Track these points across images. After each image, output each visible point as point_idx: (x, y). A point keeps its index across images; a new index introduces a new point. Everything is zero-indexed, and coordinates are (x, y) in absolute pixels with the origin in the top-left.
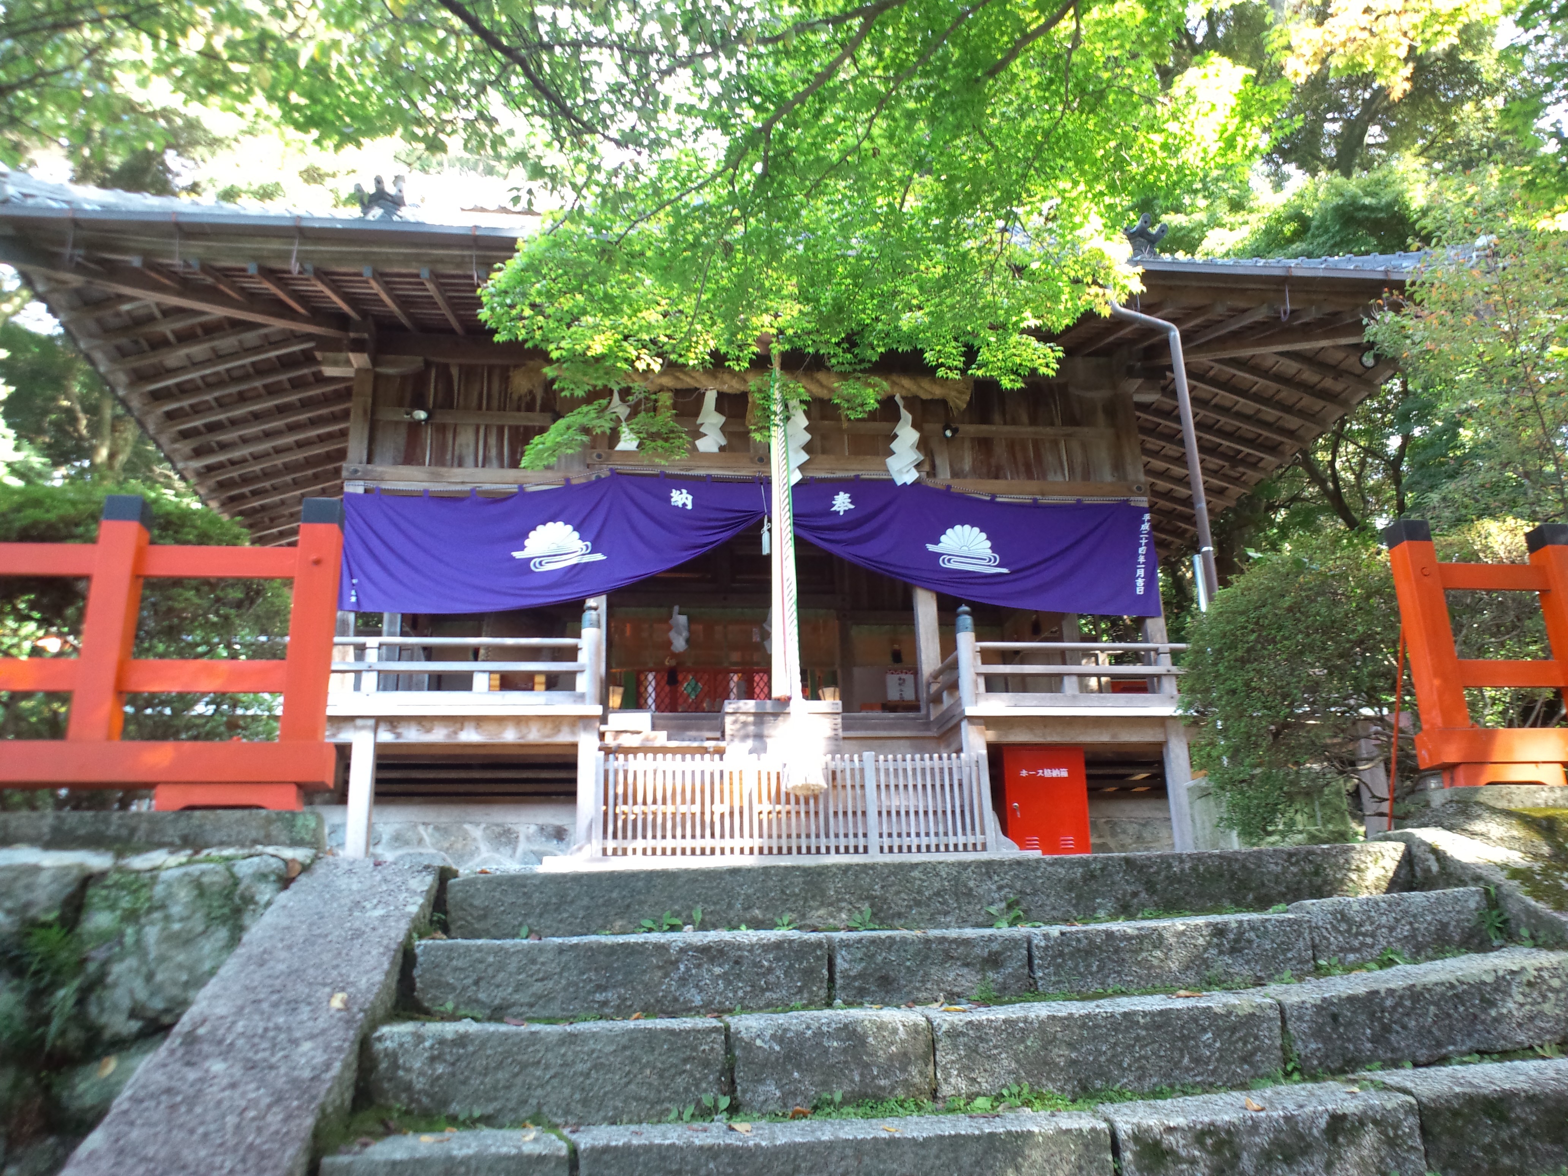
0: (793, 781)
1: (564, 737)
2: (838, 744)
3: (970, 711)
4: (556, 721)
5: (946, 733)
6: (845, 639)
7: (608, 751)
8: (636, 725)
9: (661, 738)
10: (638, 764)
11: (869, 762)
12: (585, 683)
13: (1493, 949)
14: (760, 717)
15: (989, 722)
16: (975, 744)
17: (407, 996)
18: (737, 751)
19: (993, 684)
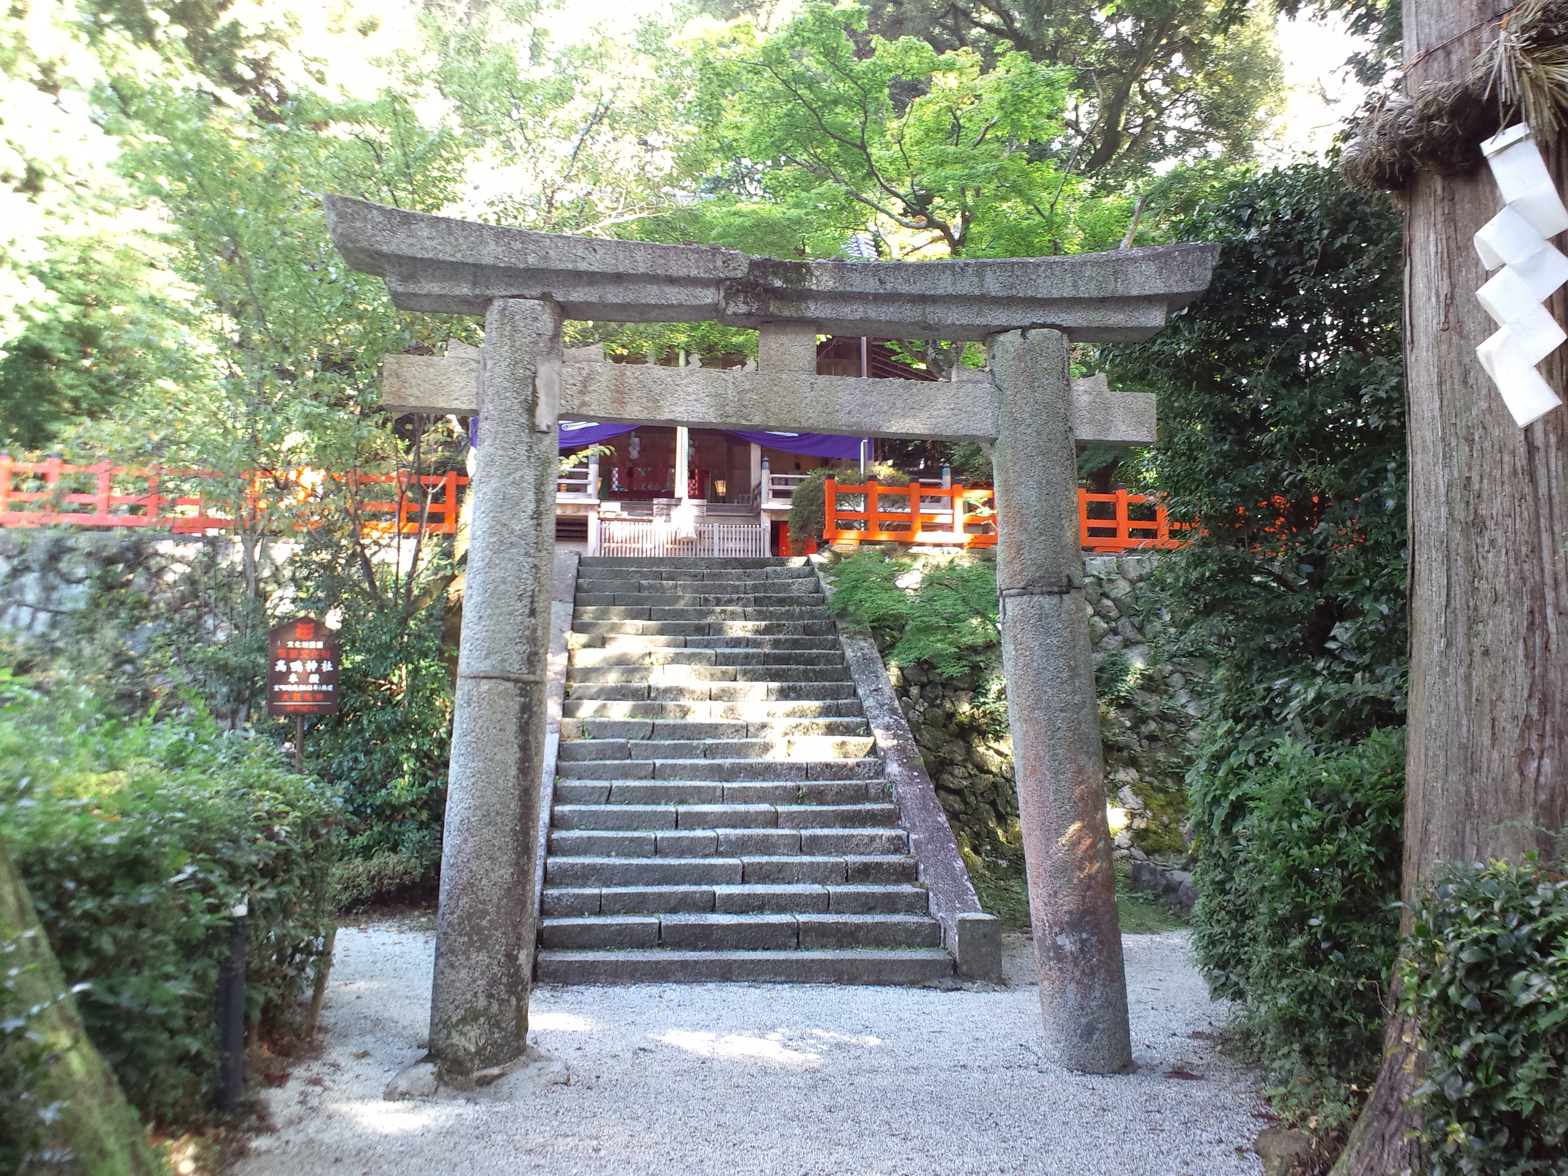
0: (682, 535)
1: (582, 513)
2: (701, 519)
3: (764, 506)
4: (579, 506)
5: (755, 514)
6: (730, 452)
7: (602, 520)
8: (613, 507)
9: (625, 515)
10: (614, 525)
11: (716, 528)
12: (590, 489)
13: (1401, 389)
14: (669, 506)
15: (772, 512)
16: (766, 522)
17: (578, 576)
18: (659, 521)
19: (777, 494)
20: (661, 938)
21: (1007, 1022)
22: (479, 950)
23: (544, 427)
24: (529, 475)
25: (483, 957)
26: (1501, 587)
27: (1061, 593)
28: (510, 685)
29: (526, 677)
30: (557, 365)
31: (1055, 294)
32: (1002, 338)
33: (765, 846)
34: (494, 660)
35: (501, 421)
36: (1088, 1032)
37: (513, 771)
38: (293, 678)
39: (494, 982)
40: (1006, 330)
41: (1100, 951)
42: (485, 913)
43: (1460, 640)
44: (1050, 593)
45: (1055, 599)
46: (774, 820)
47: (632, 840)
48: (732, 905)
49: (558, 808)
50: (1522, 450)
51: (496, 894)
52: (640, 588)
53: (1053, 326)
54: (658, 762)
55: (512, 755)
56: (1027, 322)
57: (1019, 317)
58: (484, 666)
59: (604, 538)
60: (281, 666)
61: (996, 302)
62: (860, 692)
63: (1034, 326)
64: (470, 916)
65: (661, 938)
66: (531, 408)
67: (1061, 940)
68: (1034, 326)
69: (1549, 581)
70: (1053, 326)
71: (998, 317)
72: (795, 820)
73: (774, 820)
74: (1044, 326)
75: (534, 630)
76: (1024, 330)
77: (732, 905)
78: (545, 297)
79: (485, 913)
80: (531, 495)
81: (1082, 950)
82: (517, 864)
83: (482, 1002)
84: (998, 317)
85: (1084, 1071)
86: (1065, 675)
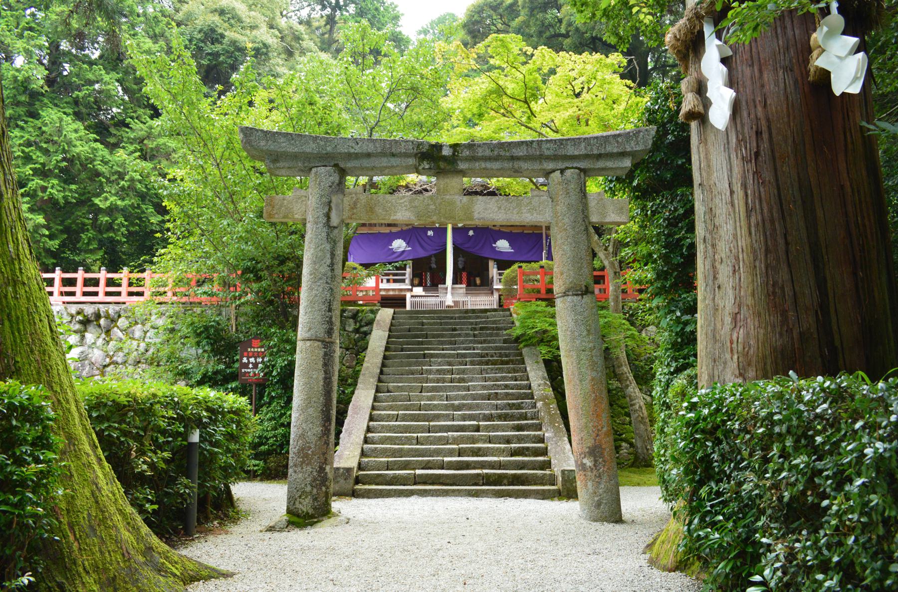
1: (403, 293)
4: (401, 290)
12: (407, 281)
20: (417, 480)
21: (570, 510)
22: (307, 465)
23: (335, 224)
24: (328, 247)
25: (309, 469)
26: (723, 256)
27: (582, 295)
28: (320, 343)
29: (327, 340)
30: (341, 196)
31: (576, 153)
32: (552, 175)
33: (473, 440)
34: (312, 332)
35: (316, 223)
36: (598, 505)
37: (322, 383)
38: (251, 366)
39: (315, 480)
40: (554, 171)
41: (604, 466)
42: (310, 448)
43: (710, 282)
44: (577, 295)
45: (580, 297)
46: (477, 429)
47: (406, 437)
48: (451, 466)
49: (371, 423)
50: (728, 193)
51: (314, 439)
52: (423, 324)
53: (576, 168)
54: (422, 403)
55: (321, 375)
56: (563, 167)
57: (561, 165)
58: (307, 335)
59: (412, 304)
60: (245, 360)
61: (548, 158)
62: (528, 369)
63: (567, 168)
64: (303, 449)
65: (417, 480)
66: (328, 216)
67: (585, 461)
68: (567, 168)
69: (740, 250)
70: (576, 168)
71: (550, 166)
72: (487, 429)
73: (477, 429)
74: (572, 168)
75: (331, 318)
76: (562, 171)
77: (451, 466)
78: (336, 165)
79: (310, 448)
80: (328, 256)
81: (594, 465)
82: (324, 426)
83: (308, 489)
84: (550, 166)
85: (595, 521)
86: (585, 333)
